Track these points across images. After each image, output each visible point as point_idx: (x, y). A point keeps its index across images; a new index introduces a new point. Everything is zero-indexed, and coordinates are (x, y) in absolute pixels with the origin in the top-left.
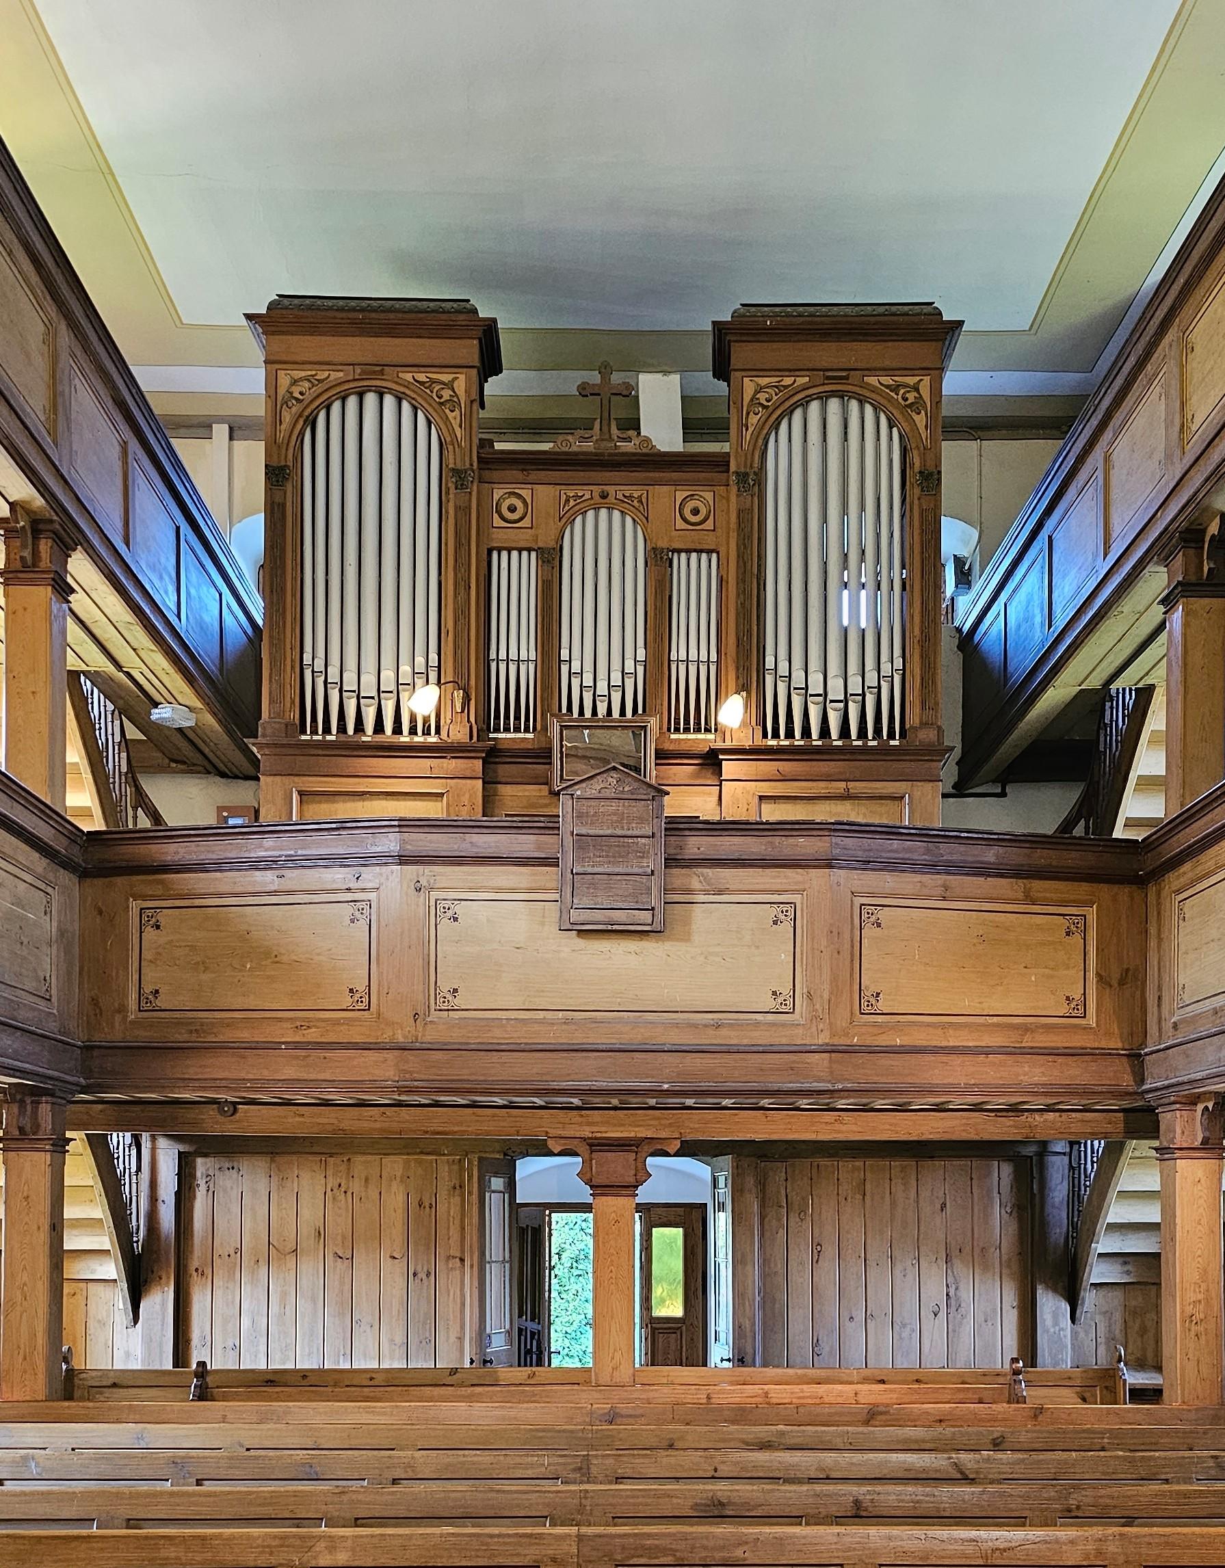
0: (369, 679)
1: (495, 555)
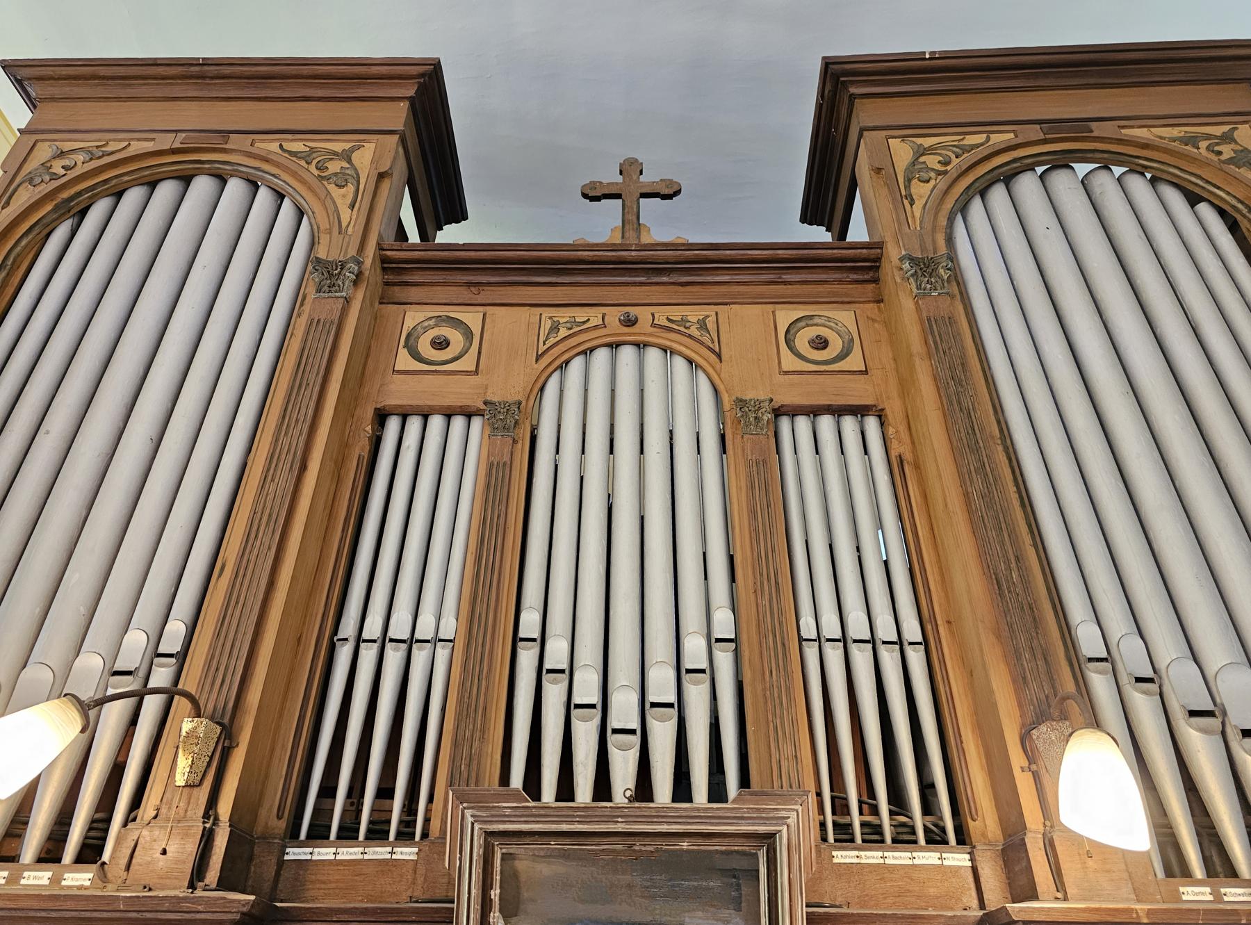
1: (393, 424)
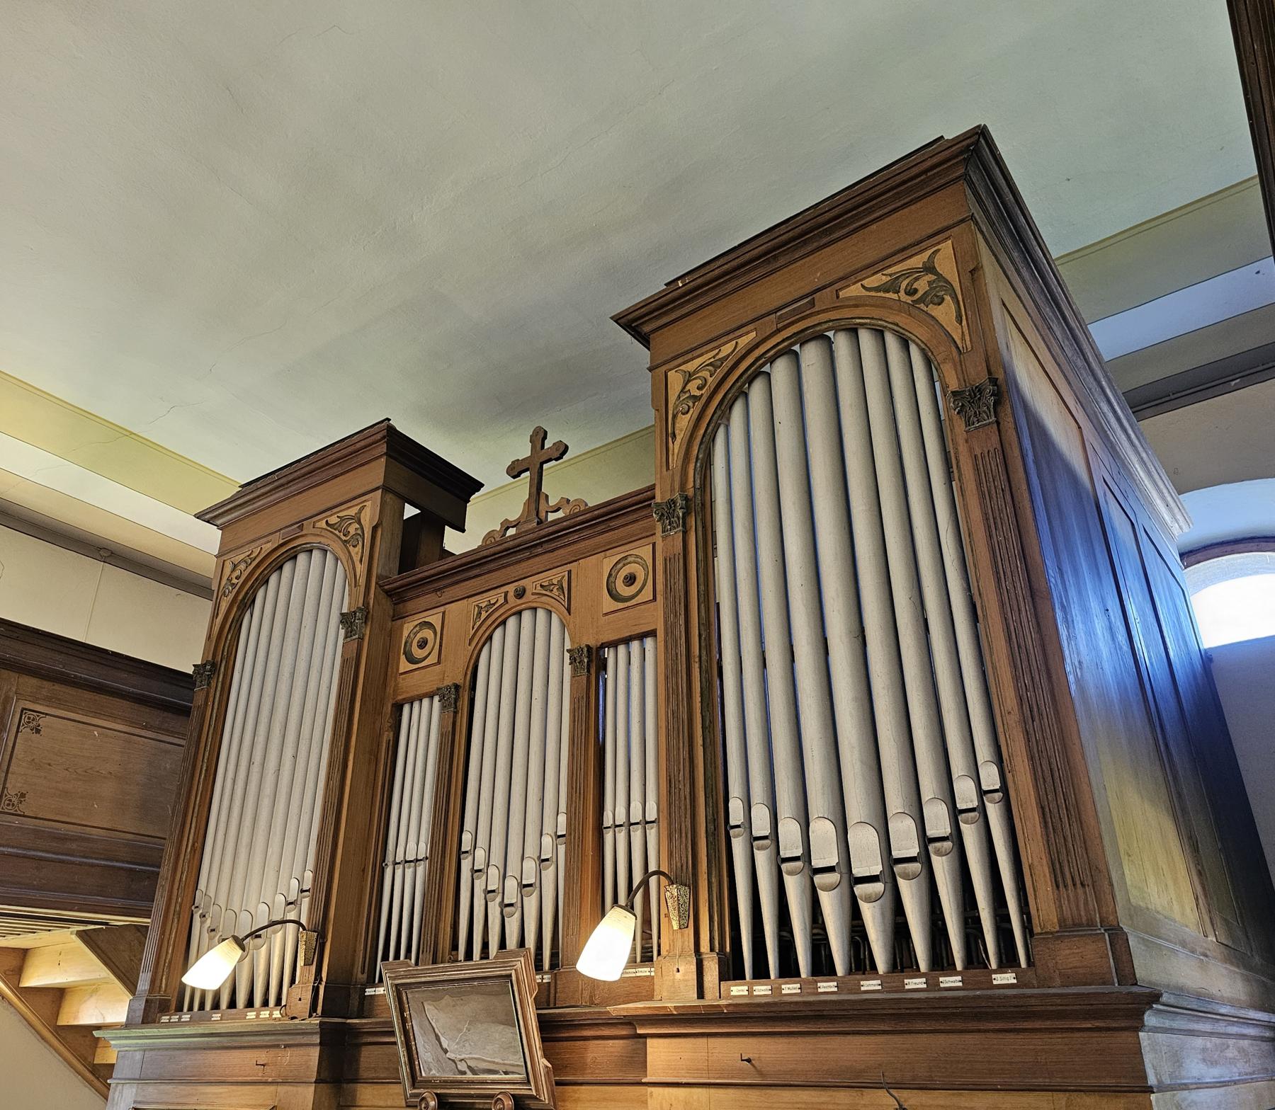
0: (864, 841)
1: (406, 708)
